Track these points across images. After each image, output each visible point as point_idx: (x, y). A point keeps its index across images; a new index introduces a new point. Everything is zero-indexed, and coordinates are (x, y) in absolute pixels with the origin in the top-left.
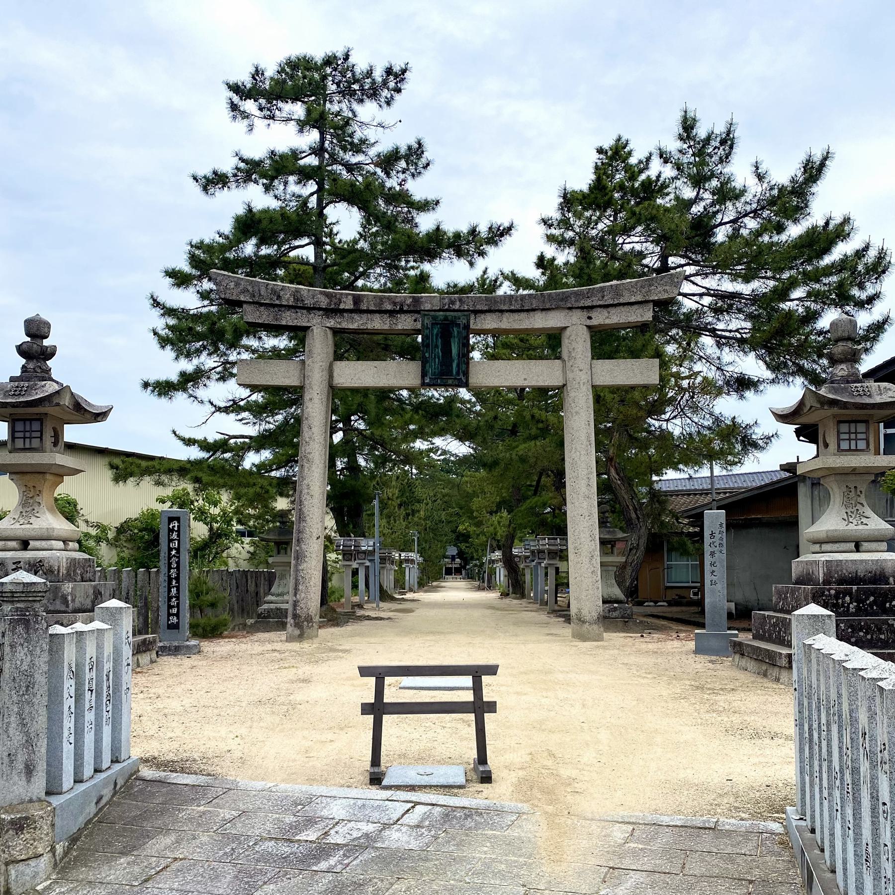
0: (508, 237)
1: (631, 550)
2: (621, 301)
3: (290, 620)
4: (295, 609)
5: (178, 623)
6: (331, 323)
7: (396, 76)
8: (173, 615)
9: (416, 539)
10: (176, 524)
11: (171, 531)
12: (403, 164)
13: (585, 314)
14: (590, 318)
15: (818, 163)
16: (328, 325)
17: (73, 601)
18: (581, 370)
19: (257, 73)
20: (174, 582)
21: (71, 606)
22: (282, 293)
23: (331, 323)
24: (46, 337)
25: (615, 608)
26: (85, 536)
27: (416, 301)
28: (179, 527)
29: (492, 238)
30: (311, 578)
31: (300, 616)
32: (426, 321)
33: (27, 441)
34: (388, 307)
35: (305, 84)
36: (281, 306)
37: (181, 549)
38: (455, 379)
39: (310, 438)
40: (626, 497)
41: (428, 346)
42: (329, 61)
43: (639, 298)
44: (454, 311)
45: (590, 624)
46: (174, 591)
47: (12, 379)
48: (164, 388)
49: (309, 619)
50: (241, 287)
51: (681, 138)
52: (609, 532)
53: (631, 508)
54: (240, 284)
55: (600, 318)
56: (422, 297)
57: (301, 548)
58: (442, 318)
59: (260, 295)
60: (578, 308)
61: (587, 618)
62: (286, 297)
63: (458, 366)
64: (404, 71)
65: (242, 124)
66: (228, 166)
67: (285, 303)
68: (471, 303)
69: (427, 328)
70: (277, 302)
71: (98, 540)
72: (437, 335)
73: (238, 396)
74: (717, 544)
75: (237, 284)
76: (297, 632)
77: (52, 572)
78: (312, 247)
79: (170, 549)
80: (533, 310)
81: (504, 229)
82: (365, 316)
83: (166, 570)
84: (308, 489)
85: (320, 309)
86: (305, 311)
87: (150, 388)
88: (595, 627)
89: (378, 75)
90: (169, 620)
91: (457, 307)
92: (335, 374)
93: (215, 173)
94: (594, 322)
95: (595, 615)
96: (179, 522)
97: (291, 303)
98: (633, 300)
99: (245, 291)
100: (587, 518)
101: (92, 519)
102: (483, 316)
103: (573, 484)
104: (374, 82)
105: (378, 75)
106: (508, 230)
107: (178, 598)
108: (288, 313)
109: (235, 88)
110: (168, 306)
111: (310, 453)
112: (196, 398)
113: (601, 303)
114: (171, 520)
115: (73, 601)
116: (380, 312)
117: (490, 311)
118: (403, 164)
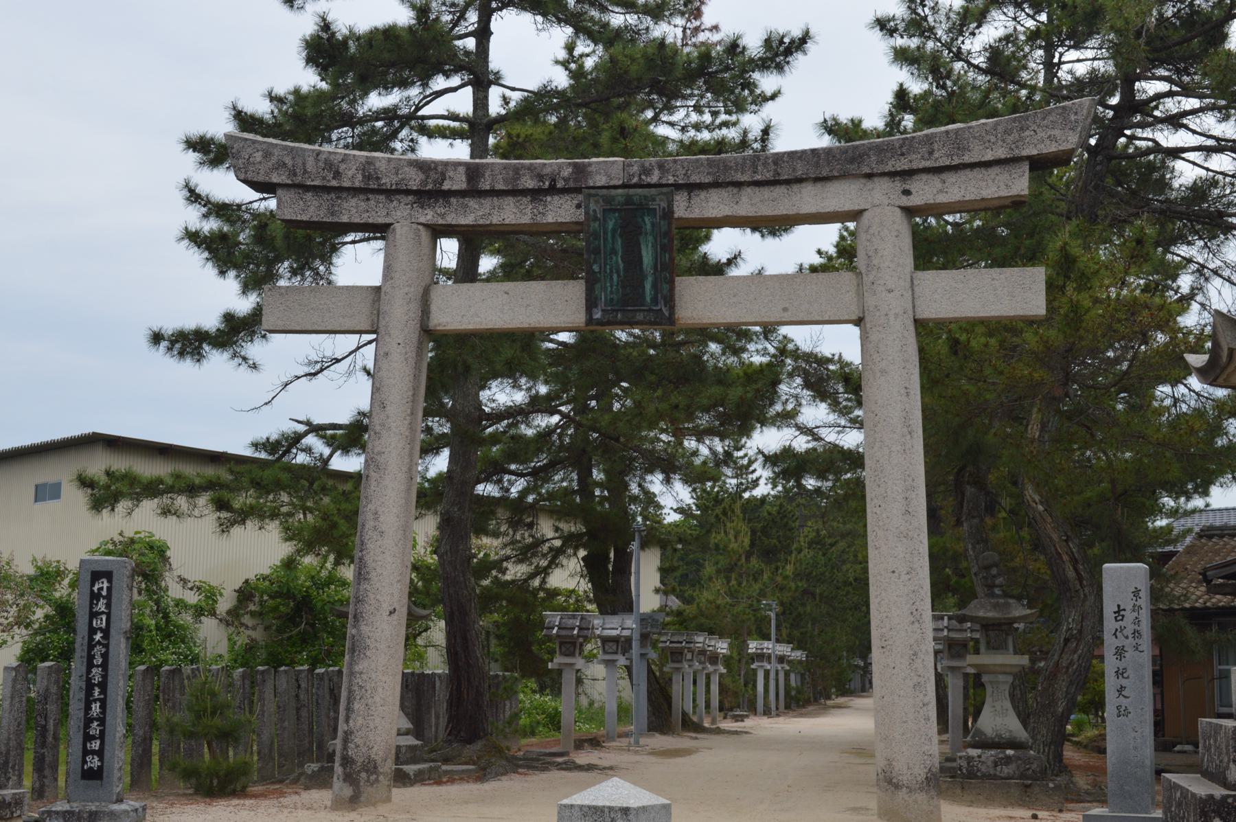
0: (799, 56)
1: (1067, 641)
2: (967, 159)
3: (338, 769)
4: (345, 748)
5: (101, 768)
6: (428, 216)
8: (93, 752)
9: (773, 615)
10: (106, 585)
13: (898, 185)
14: (907, 193)
16: (422, 220)
18: (890, 291)
20: (97, 691)
22: (342, 167)
25: (1009, 758)
26: (177, 605)
27: (580, 171)
28: (109, 589)
29: (772, 59)
30: (375, 689)
31: (353, 762)
32: (592, 206)
34: (529, 183)
37: (112, 632)
38: (650, 310)
39: (382, 425)
40: (1055, 536)
41: (597, 251)
43: (1001, 153)
44: (649, 186)
45: (910, 790)
46: (96, 708)
48: (189, 344)
49: (371, 767)
50: (274, 159)
52: (995, 606)
53: (1065, 558)
54: (271, 154)
55: (925, 192)
56: (590, 164)
57: (359, 630)
58: (621, 199)
59: (305, 172)
60: (883, 174)
61: (905, 779)
62: (350, 173)
67: (346, 184)
68: (681, 172)
69: (596, 219)
70: (334, 183)
71: (199, 612)
72: (614, 231)
73: (328, 353)
74: (1128, 632)
75: (267, 155)
76: (348, 791)
78: (469, 89)
79: (92, 631)
80: (799, 181)
81: (792, 42)
82: (487, 202)
83: (84, 669)
84: (376, 519)
85: (408, 192)
86: (382, 198)
87: (164, 344)
88: (921, 797)
90: (84, 762)
91: (654, 178)
94: (915, 200)
95: (920, 773)
96: (110, 581)
97: (357, 184)
98: (989, 156)
99: (281, 165)
100: (905, 577)
101: (193, 576)
102: (703, 194)
103: (878, 510)
106: (800, 43)
107: (102, 721)
108: (353, 202)
110: (212, 200)
111: (380, 453)
112: (245, 359)
113: (928, 164)
116: (515, 193)
117: (716, 185)
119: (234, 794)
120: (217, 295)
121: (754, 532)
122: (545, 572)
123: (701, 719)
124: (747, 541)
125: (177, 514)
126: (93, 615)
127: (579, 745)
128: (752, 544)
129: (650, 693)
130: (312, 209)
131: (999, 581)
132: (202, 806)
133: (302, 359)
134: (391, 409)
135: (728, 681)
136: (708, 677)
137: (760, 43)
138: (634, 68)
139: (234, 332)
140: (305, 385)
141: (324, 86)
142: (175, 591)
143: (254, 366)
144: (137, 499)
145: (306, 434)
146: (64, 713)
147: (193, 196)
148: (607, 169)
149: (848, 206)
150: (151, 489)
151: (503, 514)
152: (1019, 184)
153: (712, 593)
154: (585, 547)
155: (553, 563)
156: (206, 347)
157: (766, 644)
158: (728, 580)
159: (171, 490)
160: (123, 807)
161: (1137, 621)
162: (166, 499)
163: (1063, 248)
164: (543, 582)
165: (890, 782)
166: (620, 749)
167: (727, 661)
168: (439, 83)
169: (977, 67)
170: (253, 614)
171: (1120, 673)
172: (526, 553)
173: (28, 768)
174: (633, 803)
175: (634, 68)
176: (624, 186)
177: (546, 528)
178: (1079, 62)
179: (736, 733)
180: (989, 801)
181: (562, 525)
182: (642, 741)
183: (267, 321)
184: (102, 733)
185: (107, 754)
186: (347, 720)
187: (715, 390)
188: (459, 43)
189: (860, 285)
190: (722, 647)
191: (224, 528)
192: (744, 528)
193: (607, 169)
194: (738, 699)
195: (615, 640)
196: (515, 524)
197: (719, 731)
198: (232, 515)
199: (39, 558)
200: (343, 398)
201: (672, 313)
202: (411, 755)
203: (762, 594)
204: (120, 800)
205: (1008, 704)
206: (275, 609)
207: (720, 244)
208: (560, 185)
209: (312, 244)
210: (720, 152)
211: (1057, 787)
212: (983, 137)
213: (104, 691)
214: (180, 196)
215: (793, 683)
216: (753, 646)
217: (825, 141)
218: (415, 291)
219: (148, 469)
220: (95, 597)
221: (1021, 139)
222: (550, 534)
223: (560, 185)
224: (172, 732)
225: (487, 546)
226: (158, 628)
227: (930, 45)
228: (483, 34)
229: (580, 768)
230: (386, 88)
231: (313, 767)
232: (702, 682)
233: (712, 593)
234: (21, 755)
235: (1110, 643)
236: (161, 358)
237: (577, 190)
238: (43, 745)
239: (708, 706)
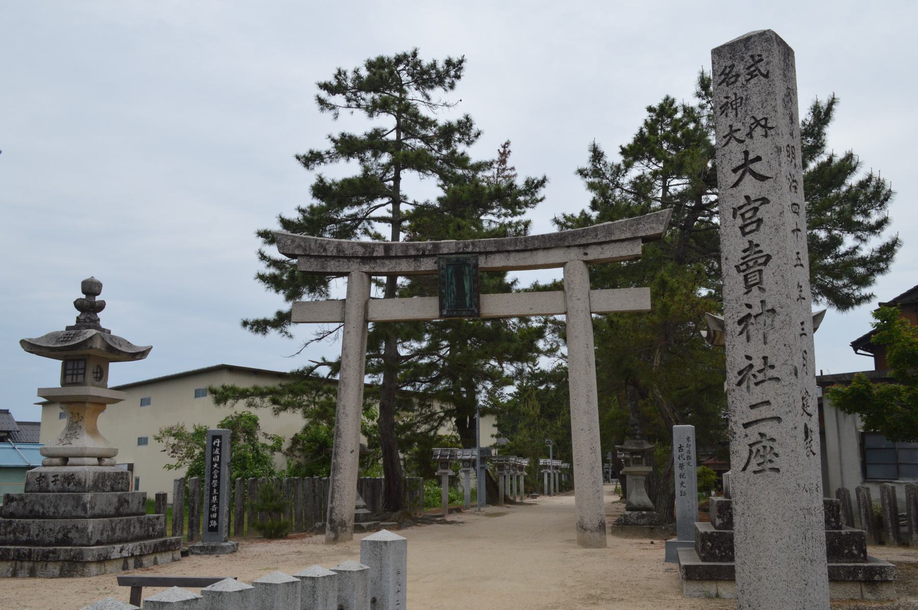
2: (613, 238)
3: (328, 525)
4: (331, 515)
5: (217, 526)
7: (455, 67)
8: (214, 519)
9: (551, 446)
11: (214, 447)
12: (457, 136)
13: (582, 251)
14: (586, 254)
15: (825, 108)
17: (92, 508)
19: (340, 74)
20: (215, 491)
21: (89, 512)
23: (367, 268)
24: (98, 294)
27: (436, 246)
28: (220, 444)
29: (529, 190)
31: (335, 522)
32: (441, 263)
33: (75, 377)
35: (382, 81)
36: (327, 256)
37: (222, 463)
40: (668, 410)
42: (399, 60)
43: (629, 235)
46: (215, 498)
47: (68, 328)
48: (261, 326)
49: (343, 524)
50: (296, 243)
51: (699, 95)
52: (636, 444)
55: (595, 254)
60: (575, 246)
61: (589, 526)
63: (471, 299)
64: (461, 62)
65: (329, 114)
66: (326, 146)
67: (329, 254)
69: (443, 269)
70: (324, 254)
71: (273, 449)
74: (685, 457)
75: (293, 241)
76: (332, 535)
77: (80, 484)
79: (213, 463)
80: (536, 249)
81: (538, 182)
82: (394, 261)
85: (357, 257)
86: (346, 260)
87: (249, 326)
88: (597, 534)
89: (441, 65)
91: (470, 249)
92: (370, 310)
93: (311, 152)
94: (590, 257)
98: (623, 237)
99: (299, 246)
100: (587, 432)
101: (271, 432)
102: (492, 256)
104: (438, 72)
105: (441, 65)
107: (217, 505)
108: (332, 262)
109: (325, 86)
112: (286, 333)
113: (595, 241)
114: (215, 438)
115: (92, 508)
117: (498, 252)
118: (457, 136)
119: (282, 537)
120: (275, 302)
121: (543, 406)
122: (436, 428)
123: (515, 498)
124: (538, 410)
125: (256, 406)
126: (213, 456)
127: (451, 511)
128: (542, 411)
129: (487, 486)
130: (312, 266)
131: (638, 432)
132: (265, 543)
133: (314, 332)
134: (350, 358)
135: (529, 479)
136: (518, 477)
137: (523, 183)
138: (464, 195)
139: (282, 320)
140: (312, 346)
141: (324, 204)
142: (262, 440)
143: (291, 336)
144: (237, 399)
145: (316, 367)
146: (201, 503)
147: (263, 257)
148: (449, 245)
149: (559, 261)
150: (243, 394)
151: (415, 400)
152: (637, 249)
153: (523, 436)
154: (455, 416)
155: (440, 424)
156: (269, 328)
157: (548, 460)
158: (530, 429)
159: (252, 394)
160: (227, 544)
161: (689, 452)
162: (250, 399)
163: (661, 277)
164: (435, 433)
165: (582, 527)
166: (471, 513)
167: (528, 469)
168: (379, 201)
169: (626, 191)
170: (299, 450)
171: (681, 476)
172: (428, 419)
173: (186, 525)
174: (389, 539)
175: (464, 195)
176: (456, 253)
177: (437, 407)
178: (678, 185)
179: (530, 504)
180: (634, 536)
181: (444, 406)
182: (482, 509)
183: (293, 318)
184: (218, 510)
185: (220, 520)
186: (332, 502)
187: (506, 344)
188: (387, 183)
189: (565, 297)
190: (525, 462)
191: (276, 412)
192: (536, 403)
193: (449, 245)
194: (534, 487)
195: (469, 461)
196: (422, 406)
197: (522, 504)
198: (280, 406)
199: (197, 424)
200: (332, 350)
201: (479, 311)
202: (366, 518)
203: (546, 436)
204: (226, 541)
205: (644, 490)
206: (310, 447)
207: (510, 277)
208: (427, 253)
209: (318, 281)
210: (505, 236)
211: (667, 529)
212: (621, 226)
213: (218, 490)
214: (256, 257)
215: (563, 479)
216: (542, 462)
217: (555, 229)
218: (361, 303)
219: (244, 383)
220: (214, 447)
221: (638, 228)
222: (439, 410)
223: (427, 253)
224: (252, 508)
225: (403, 418)
226: (253, 458)
227: (605, 181)
228: (397, 179)
229: (448, 523)
230: (351, 206)
231: (319, 524)
232: (515, 479)
233: (523, 436)
234: (182, 520)
235: (677, 462)
236: (247, 332)
237: (434, 255)
238: (193, 516)
239: (518, 490)
